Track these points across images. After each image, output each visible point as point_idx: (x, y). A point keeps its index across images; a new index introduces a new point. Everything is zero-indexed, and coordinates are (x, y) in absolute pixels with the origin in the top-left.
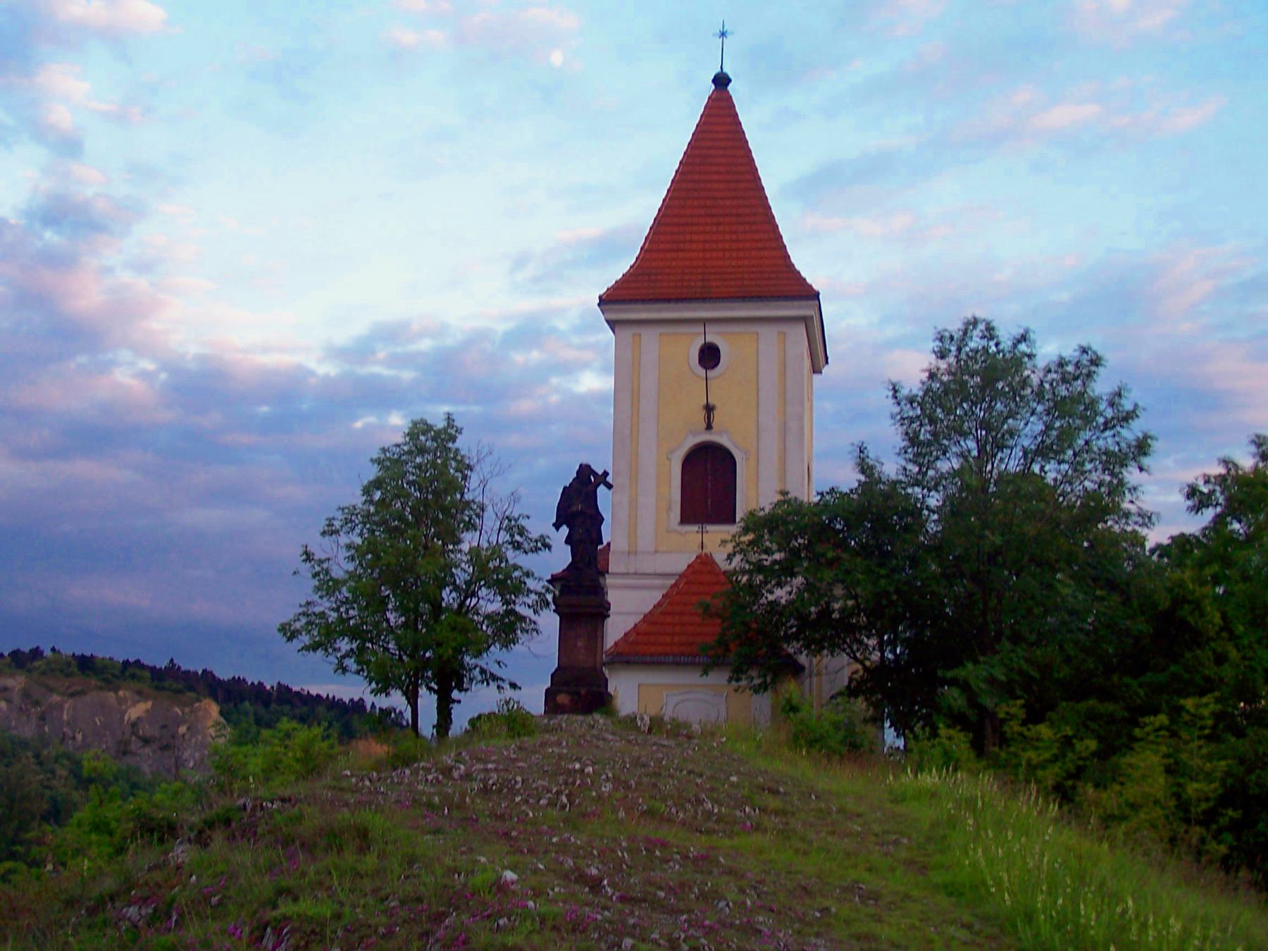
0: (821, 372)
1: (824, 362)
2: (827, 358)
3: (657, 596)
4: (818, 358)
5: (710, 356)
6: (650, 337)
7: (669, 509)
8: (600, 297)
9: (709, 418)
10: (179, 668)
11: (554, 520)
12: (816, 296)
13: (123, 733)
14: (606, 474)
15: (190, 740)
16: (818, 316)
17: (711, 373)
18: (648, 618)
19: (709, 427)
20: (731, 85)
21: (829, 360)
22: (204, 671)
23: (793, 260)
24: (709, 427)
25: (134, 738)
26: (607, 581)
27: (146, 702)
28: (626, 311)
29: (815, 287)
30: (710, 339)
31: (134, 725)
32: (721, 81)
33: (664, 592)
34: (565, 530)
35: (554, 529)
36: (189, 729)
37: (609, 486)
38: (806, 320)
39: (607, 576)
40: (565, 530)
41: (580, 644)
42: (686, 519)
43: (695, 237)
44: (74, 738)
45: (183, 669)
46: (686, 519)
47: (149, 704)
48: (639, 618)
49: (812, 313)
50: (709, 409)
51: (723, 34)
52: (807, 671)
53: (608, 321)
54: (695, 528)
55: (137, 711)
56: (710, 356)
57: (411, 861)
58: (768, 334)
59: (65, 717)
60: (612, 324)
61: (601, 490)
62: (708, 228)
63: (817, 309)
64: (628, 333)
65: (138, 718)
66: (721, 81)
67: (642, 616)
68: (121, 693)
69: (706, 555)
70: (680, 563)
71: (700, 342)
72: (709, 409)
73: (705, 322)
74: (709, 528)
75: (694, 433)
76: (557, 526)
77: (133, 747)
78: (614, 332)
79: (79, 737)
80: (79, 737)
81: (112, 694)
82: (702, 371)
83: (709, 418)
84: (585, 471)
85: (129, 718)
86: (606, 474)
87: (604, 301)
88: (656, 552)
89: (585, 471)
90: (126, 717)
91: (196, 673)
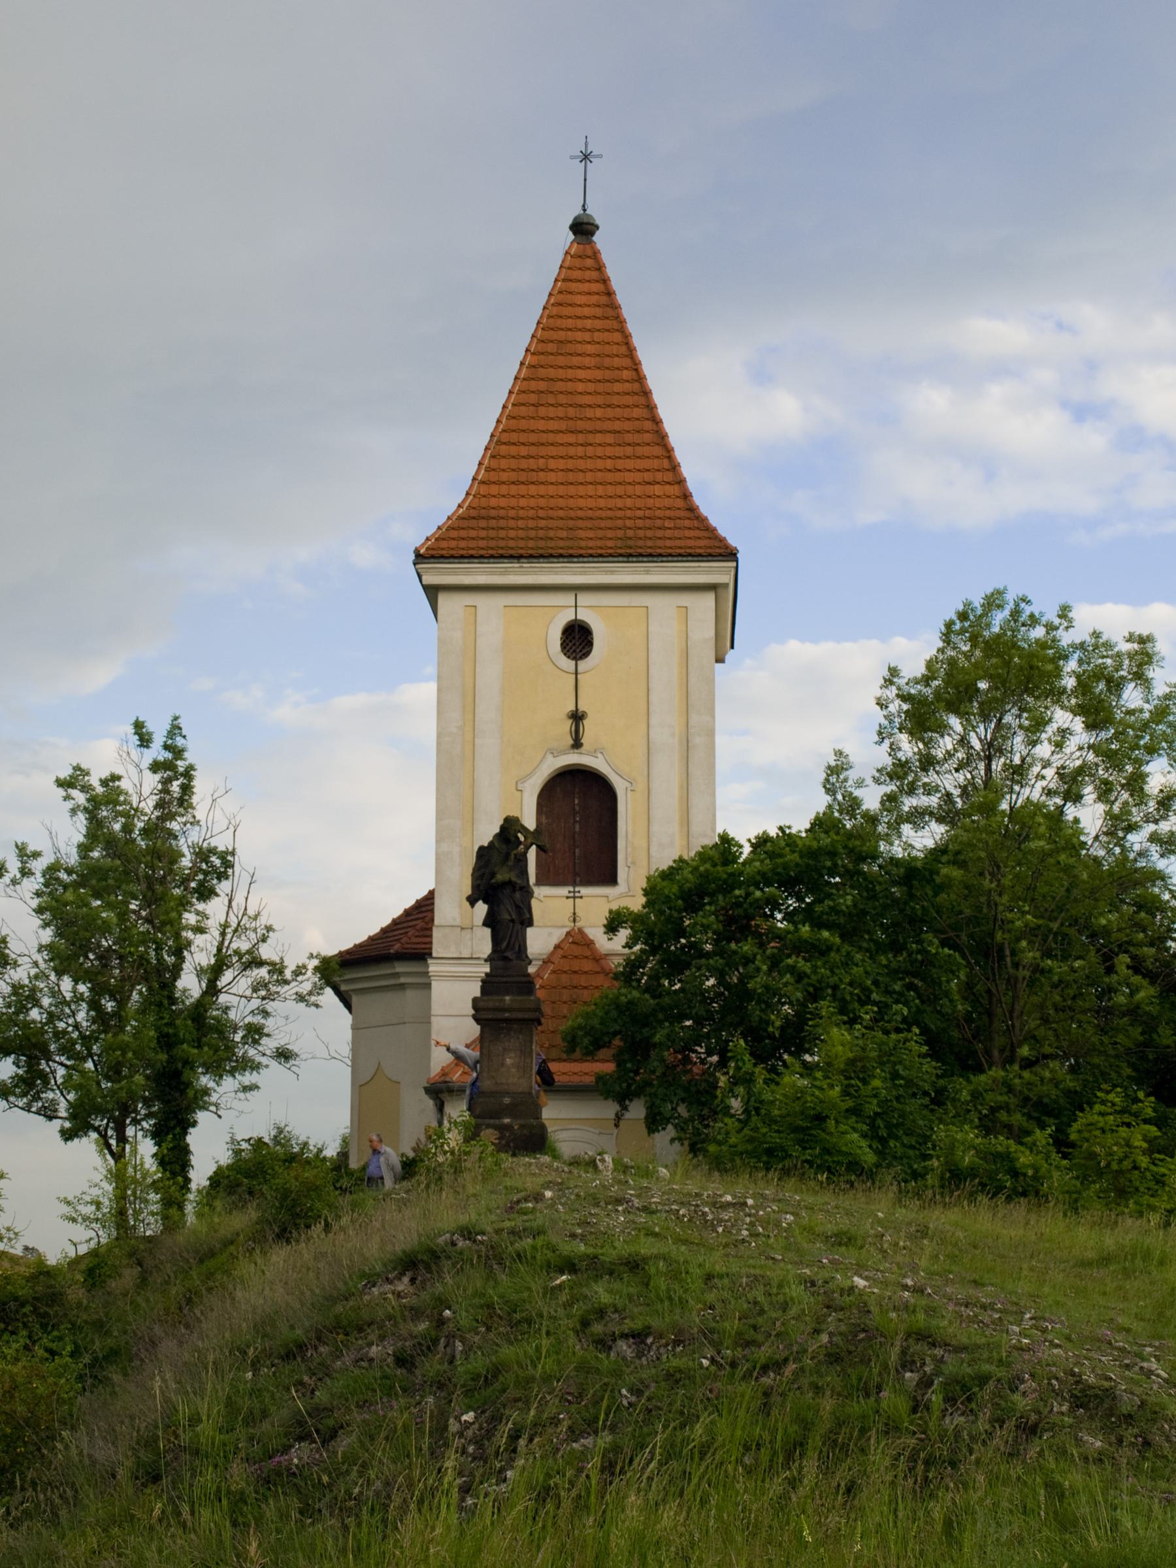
9: (577, 731)
11: (469, 892)
12: (730, 554)
17: (583, 665)
19: (577, 744)
26: (431, 969)
28: (454, 572)
29: (732, 541)
30: (584, 616)
32: (583, 228)
35: (467, 904)
39: (430, 961)
41: (508, 1061)
43: (552, 464)
50: (577, 717)
51: (586, 157)
54: (564, 891)
57: (709, 1277)
62: (630, 489)
63: (733, 573)
66: (583, 228)
71: (568, 616)
72: (577, 717)
74: (584, 891)
75: (555, 753)
82: (568, 664)
83: (577, 731)
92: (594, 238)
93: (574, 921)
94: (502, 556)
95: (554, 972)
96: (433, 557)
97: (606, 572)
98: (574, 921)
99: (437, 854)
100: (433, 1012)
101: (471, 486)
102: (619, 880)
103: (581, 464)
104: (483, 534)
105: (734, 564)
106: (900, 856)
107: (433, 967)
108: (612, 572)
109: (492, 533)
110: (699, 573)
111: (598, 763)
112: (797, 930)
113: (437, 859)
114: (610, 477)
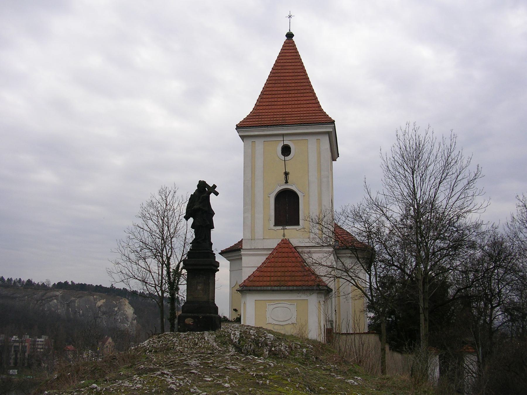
0: (336, 160)
1: (337, 156)
2: (338, 154)
3: (263, 259)
4: (335, 155)
5: (286, 150)
6: (259, 144)
7: (269, 220)
8: (237, 125)
9: (286, 178)
10: (115, 287)
13: (96, 311)
14: (215, 187)
15: (119, 312)
16: (334, 131)
17: (287, 158)
18: (259, 269)
19: (287, 182)
20: (294, 37)
21: (339, 155)
22: (123, 288)
23: (323, 107)
24: (287, 182)
25: (100, 312)
27: (103, 300)
29: (333, 118)
31: (99, 307)
32: (290, 36)
33: (267, 257)
34: (191, 220)
36: (118, 309)
37: (217, 194)
38: (328, 133)
40: (191, 220)
41: (199, 288)
42: (277, 224)
44: (79, 313)
45: (116, 288)
46: (277, 224)
47: (105, 300)
48: (255, 269)
49: (331, 130)
50: (286, 174)
52: (333, 292)
53: (239, 136)
55: (100, 303)
56: (286, 150)
58: (312, 141)
59: (76, 305)
60: (242, 137)
61: (212, 196)
64: (249, 141)
65: (101, 305)
66: (290, 36)
67: (257, 268)
68: (95, 297)
69: (285, 239)
70: (273, 244)
72: (286, 174)
73: (283, 135)
74: (287, 227)
76: (187, 218)
77: (100, 315)
78: (243, 141)
79: (81, 312)
80: (81, 312)
81: (92, 297)
83: (286, 178)
84: (202, 185)
85: (98, 305)
86: (215, 187)
87: (239, 127)
88: (264, 239)
89: (202, 185)
90: (97, 305)
91: (121, 289)
92: (293, 39)
93: (284, 236)
94: (262, 126)
95: (277, 252)
96: (241, 127)
97: (294, 129)
98: (284, 236)
99: (244, 217)
100: (186, 285)
101: (255, 107)
102: (300, 224)
103: (288, 99)
104: (257, 120)
105: (334, 125)
106: (206, 333)
107: (242, 252)
108: (296, 129)
109: (260, 120)
110: (323, 128)
111: (293, 188)
112: (482, 320)
113: (244, 218)
114: (296, 102)
